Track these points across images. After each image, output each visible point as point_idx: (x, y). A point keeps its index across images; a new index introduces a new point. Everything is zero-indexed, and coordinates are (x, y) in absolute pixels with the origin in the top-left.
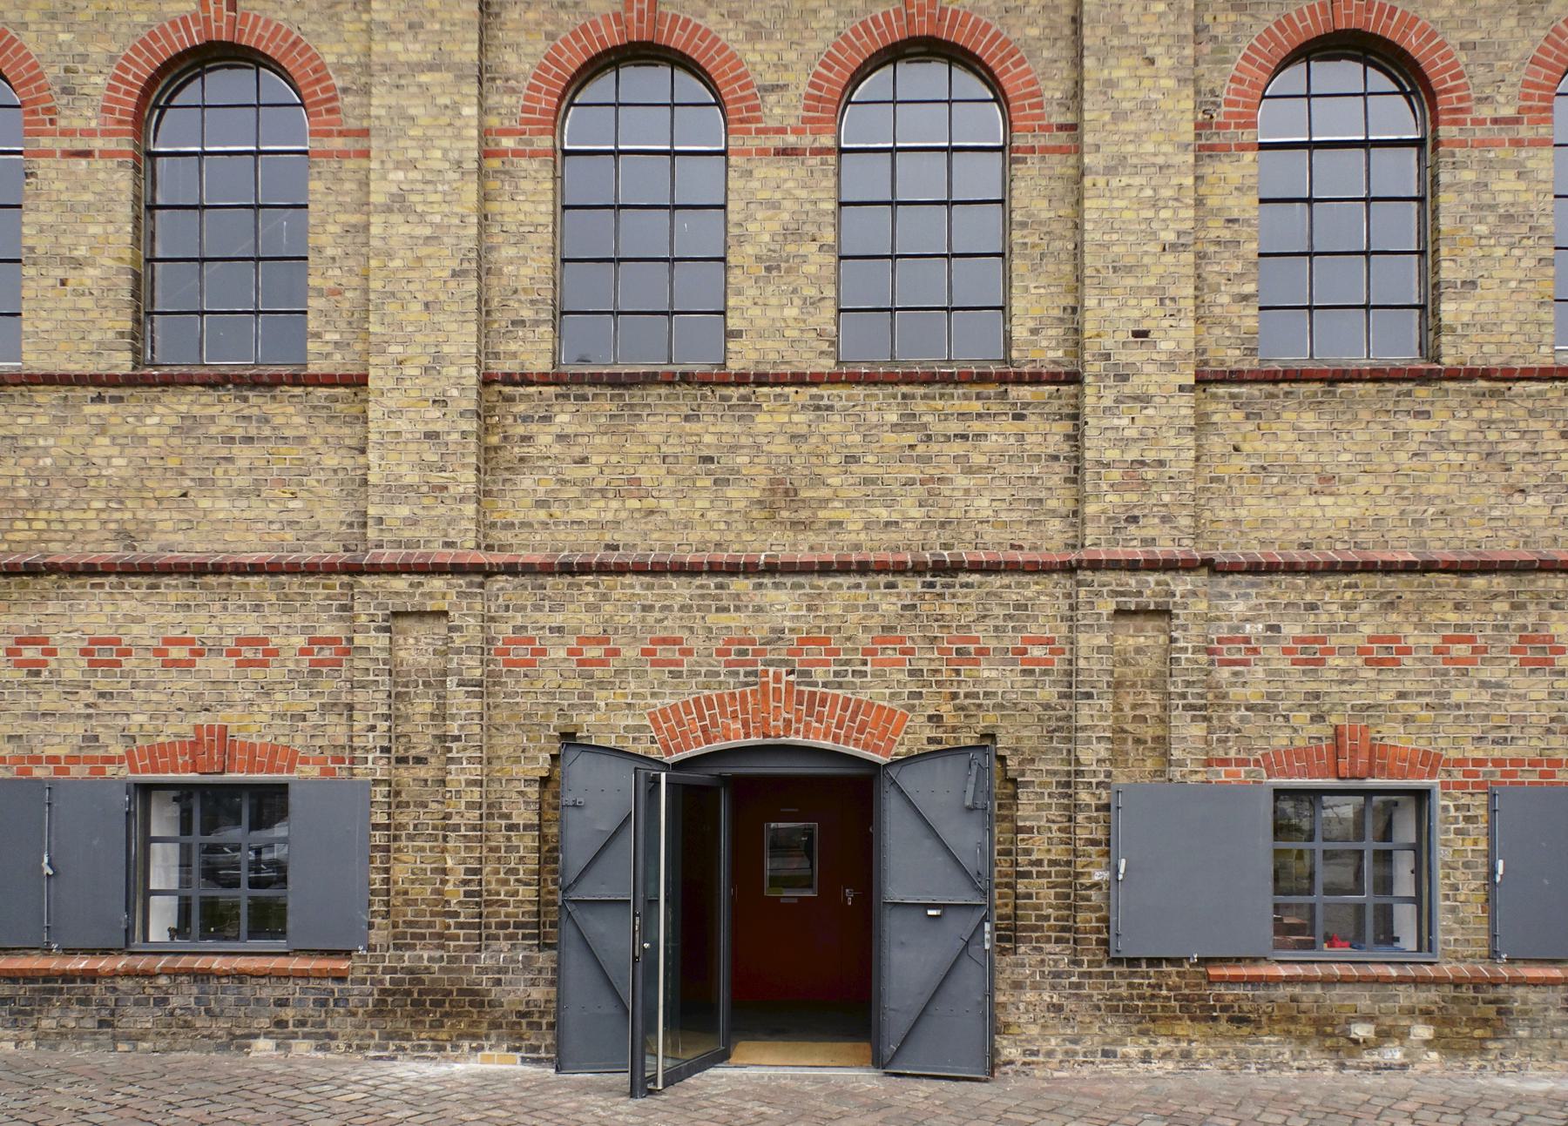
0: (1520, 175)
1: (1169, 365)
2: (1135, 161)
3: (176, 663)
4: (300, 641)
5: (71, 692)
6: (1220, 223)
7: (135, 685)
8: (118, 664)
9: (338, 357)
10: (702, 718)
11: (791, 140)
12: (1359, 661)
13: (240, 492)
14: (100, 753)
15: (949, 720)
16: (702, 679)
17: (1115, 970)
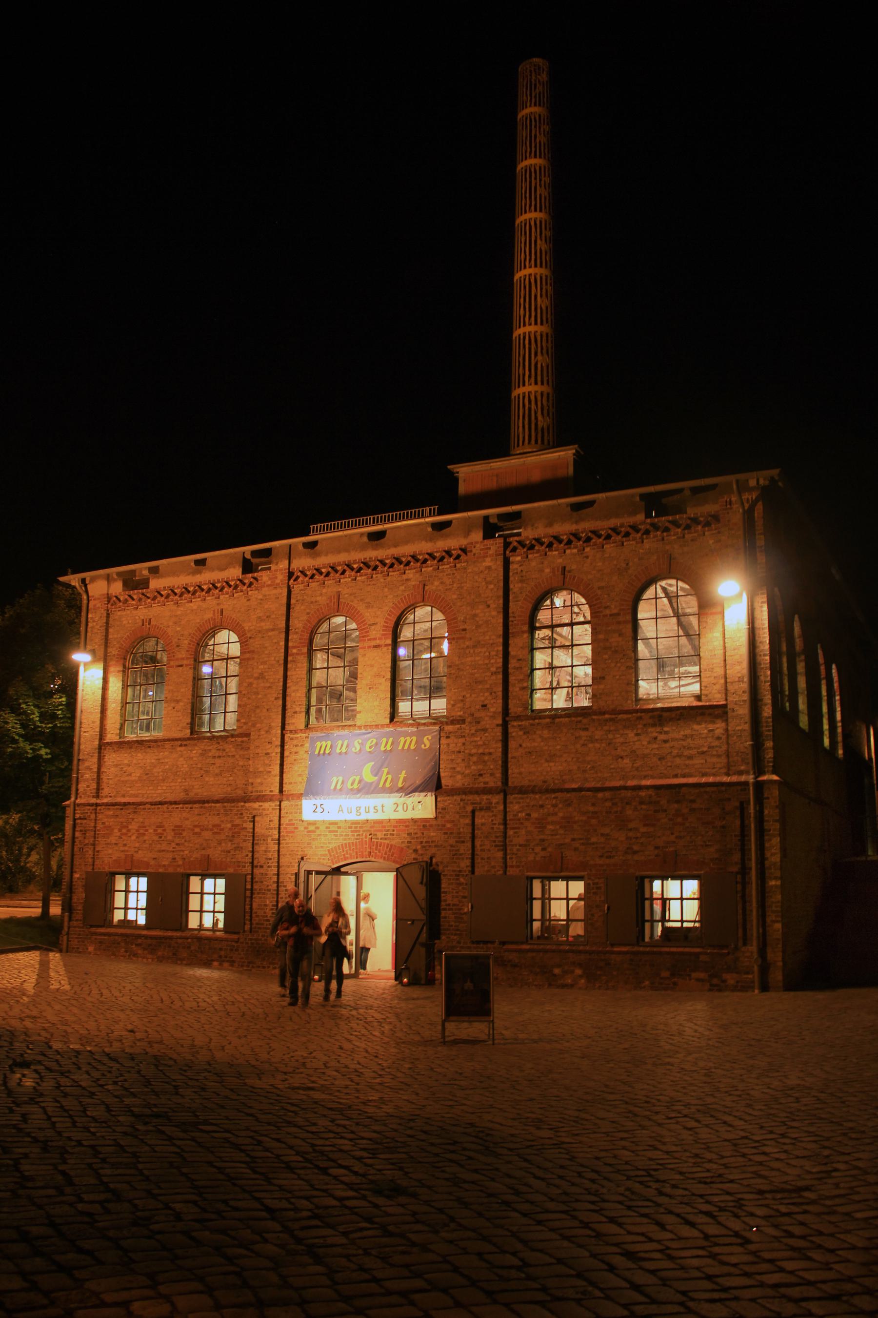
0: (620, 635)
1: (493, 717)
2: (483, 643)
3: (196, 833)
4: (229, 825)
5: (170, 842)
6: (515, 661)
7: (185, 841)
8: (181, 834)
9: (244, 727)
10: (343, 851)
11: (378, 642)
12: (558, 827)
13: (217, 775)
14: (176, 864)
15: (420, 852)
16: (344, 837)
17: (472, 945)
